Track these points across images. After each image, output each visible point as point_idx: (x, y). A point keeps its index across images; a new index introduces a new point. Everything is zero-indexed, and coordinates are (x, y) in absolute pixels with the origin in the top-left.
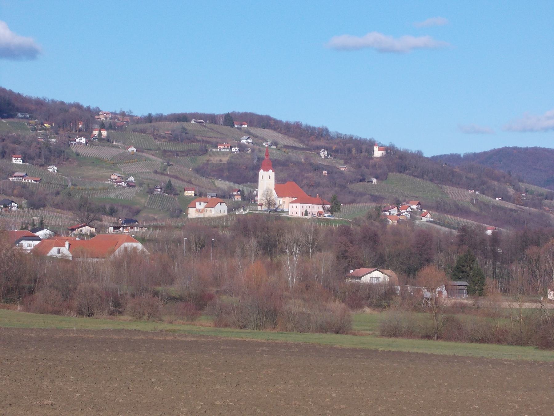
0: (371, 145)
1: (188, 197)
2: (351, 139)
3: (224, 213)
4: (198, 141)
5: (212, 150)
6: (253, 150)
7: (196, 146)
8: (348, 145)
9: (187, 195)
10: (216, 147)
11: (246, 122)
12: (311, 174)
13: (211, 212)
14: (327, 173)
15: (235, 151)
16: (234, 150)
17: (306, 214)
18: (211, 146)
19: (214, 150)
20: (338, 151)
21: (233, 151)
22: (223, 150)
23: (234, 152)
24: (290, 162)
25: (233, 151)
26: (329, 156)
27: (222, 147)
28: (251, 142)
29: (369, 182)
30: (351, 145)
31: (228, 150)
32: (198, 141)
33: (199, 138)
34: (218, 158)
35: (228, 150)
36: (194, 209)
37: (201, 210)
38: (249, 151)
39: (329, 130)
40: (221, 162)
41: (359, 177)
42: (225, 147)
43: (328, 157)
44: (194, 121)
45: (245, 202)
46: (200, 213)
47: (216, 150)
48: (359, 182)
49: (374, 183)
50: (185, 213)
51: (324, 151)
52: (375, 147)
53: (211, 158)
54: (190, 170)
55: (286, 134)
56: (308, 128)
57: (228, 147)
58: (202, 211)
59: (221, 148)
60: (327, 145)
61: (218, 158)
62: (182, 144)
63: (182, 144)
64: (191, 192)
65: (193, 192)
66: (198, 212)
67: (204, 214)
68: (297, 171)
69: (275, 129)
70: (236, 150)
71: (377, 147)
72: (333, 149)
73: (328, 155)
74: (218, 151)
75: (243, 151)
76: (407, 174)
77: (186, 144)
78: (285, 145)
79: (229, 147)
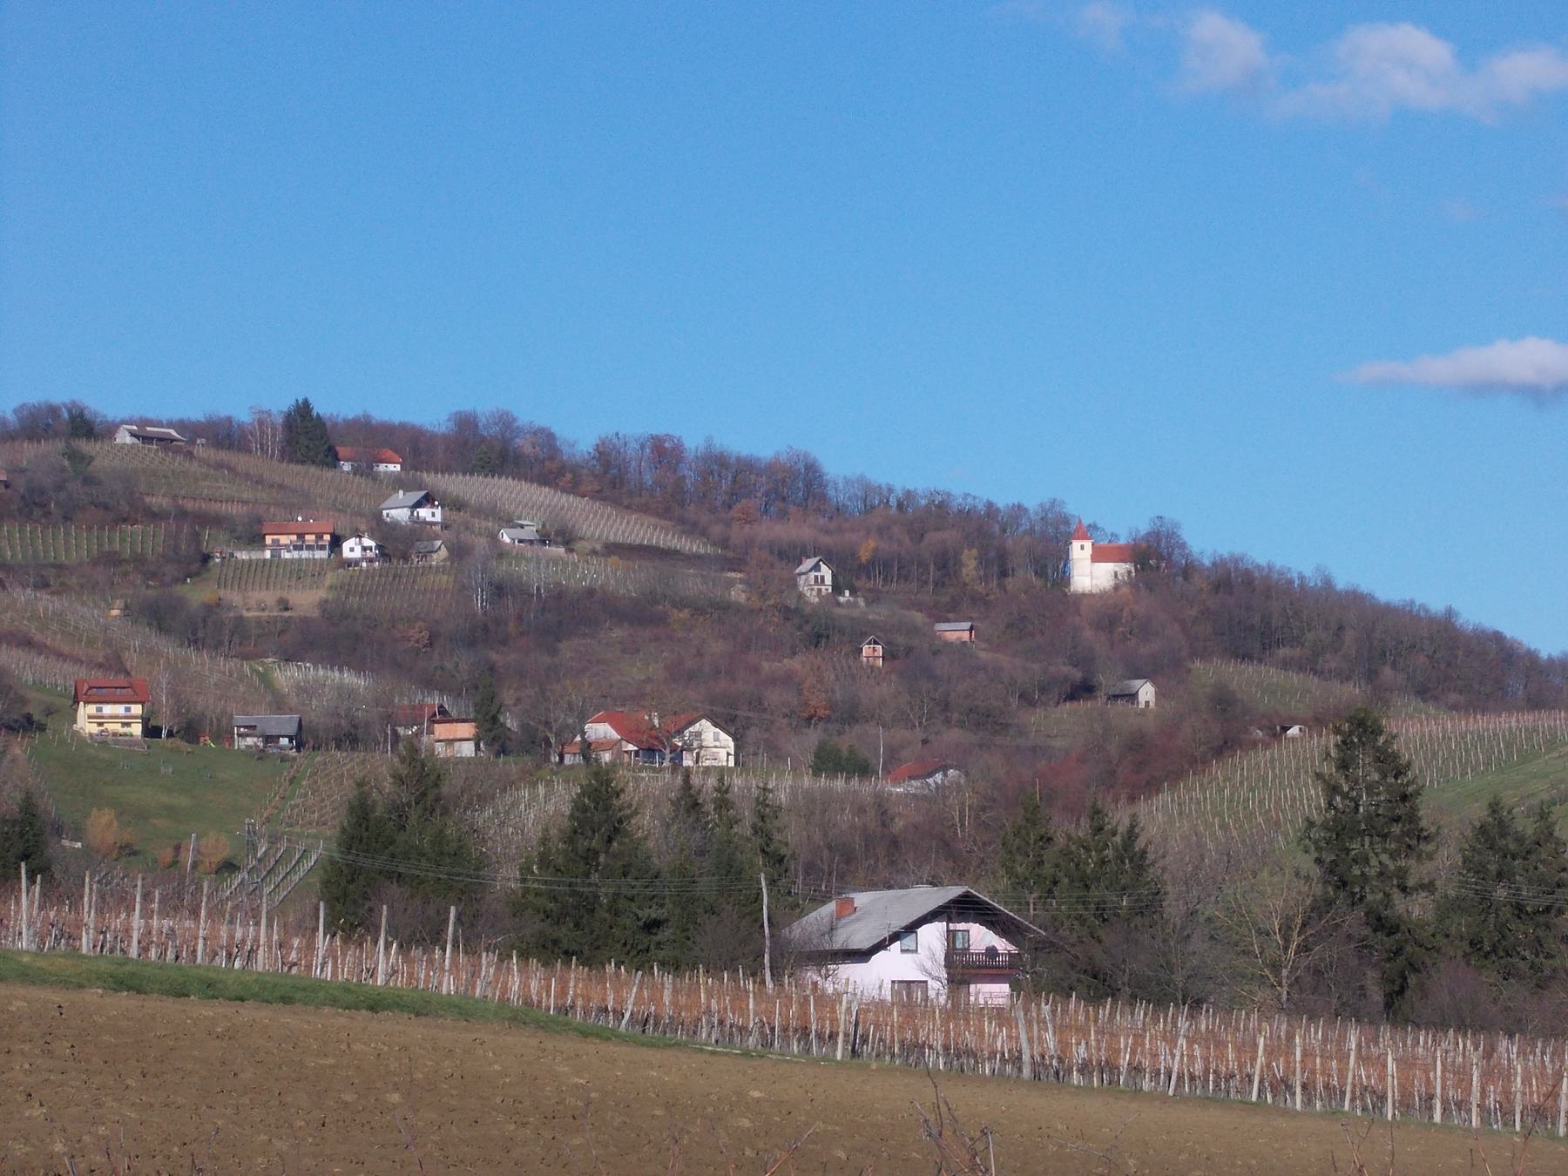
1: (103, 741)
2: (939, 512)
4: (153, 516)
5: (232, 555)
6: (459, 552)
7: (138, 538)
8: (933, 537)
9: (93, 729)
10: (256, 540)
11: (396, 450)
12: (795, 664)
14: (883, 657)
15: (358, 554)
16: (352, 550)
18: (223, 536)
19: (243, 556)
20: (887, 565)
21: (346, 553)
22: (296, 554)
23: (356, 562)
24: (674, 605)
25: (346, 553)
26: (842, 594)
27: (284, 540)
28: (438, 518)
29: (1116, 697)
30: (949, 536)
31: (323, 554)
32: (153, 516)
33: (158, 501)
34: (269, 597)
35: (323, 554)
38: (435, 556)
39: (825, 470)
40: (287, 614)
41: (1066, 669)
42: (301, 536)
43: (841, 599)
44: (127, 434)
45: (511, 765)
47: (255, 555)
48: (1065, 701)
49: (1142, 706)
50: (79, 845)
51: (816, 567)
53: (233, 597)
54: (115, 612)
55: (604, 499)
56: (716, 464)
57: (319, 537)
59: (283, 546)
60: (826, 540)
61: (269, 597)
62: (67, 534)
63: (67, 534)
64: (120, 709)
65: (137, 709)
68: (717, 647)
69: (547, 479)
70: (364, 549)
71: (1088, 544)
72: (863, 560)
73: (837, 588)
74: (265, 561)
75: (405, 557)
76: (1285, 665)
77: (90, 528)
78: (611, 538)
79: (327, 537)
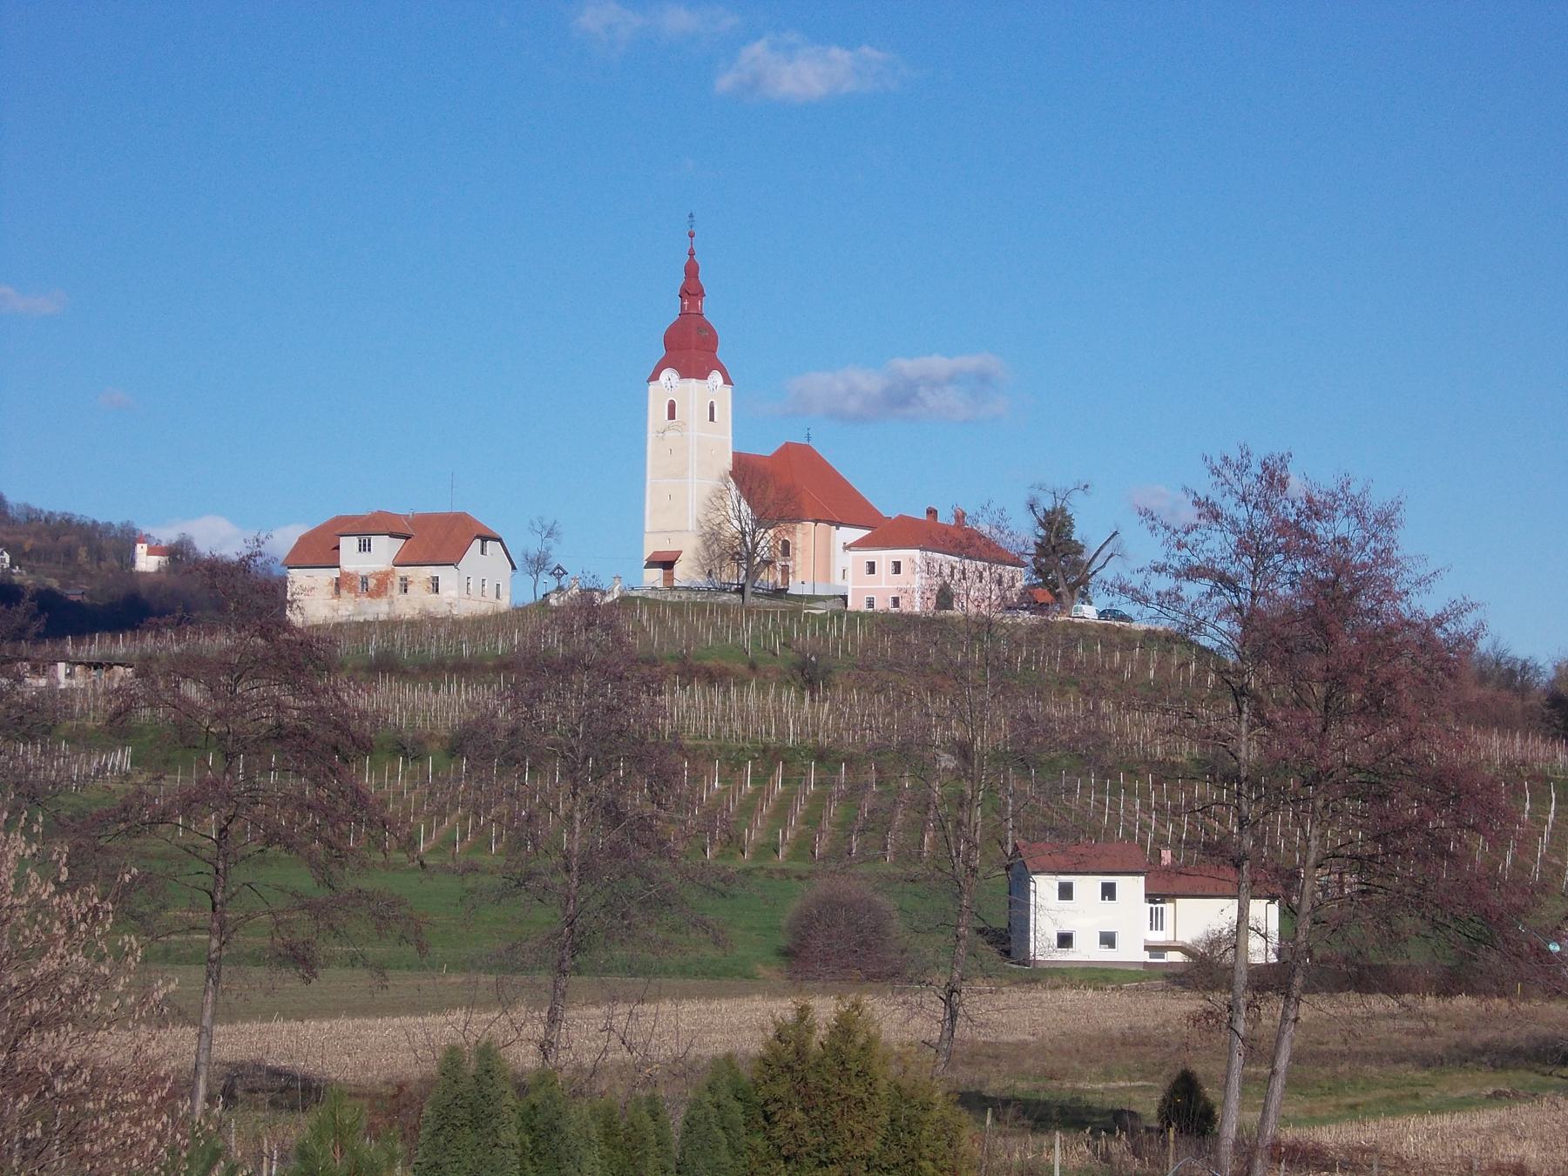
0: (126, 541)
3: (498, 597)
13: (437, 591)
17: (945, 597)
36: (326, 576)
37: (372, 583)
46: (365, 599)
52: (139, 546)
58: (376, 586)
66: (352, 589)
67: (391, 603)
71: (145, 546)
